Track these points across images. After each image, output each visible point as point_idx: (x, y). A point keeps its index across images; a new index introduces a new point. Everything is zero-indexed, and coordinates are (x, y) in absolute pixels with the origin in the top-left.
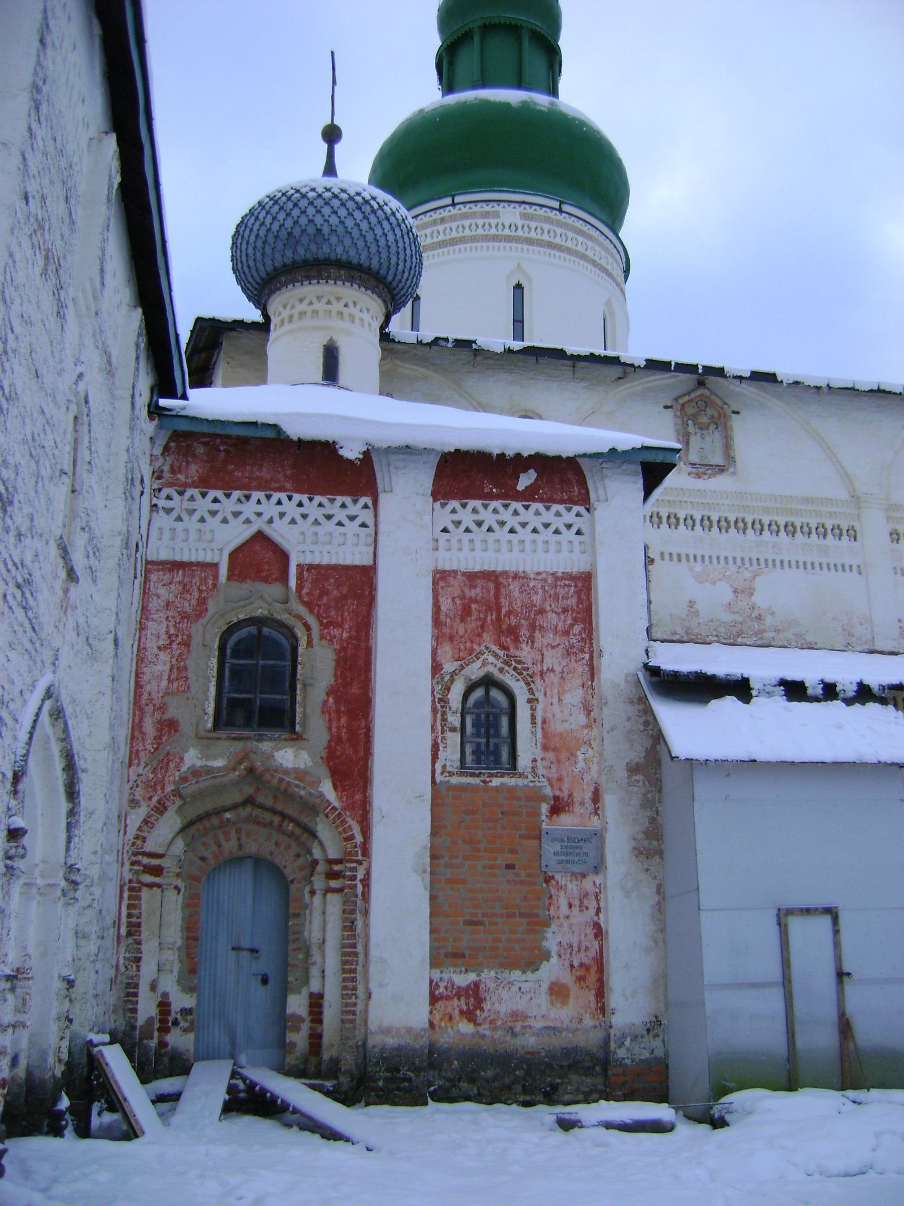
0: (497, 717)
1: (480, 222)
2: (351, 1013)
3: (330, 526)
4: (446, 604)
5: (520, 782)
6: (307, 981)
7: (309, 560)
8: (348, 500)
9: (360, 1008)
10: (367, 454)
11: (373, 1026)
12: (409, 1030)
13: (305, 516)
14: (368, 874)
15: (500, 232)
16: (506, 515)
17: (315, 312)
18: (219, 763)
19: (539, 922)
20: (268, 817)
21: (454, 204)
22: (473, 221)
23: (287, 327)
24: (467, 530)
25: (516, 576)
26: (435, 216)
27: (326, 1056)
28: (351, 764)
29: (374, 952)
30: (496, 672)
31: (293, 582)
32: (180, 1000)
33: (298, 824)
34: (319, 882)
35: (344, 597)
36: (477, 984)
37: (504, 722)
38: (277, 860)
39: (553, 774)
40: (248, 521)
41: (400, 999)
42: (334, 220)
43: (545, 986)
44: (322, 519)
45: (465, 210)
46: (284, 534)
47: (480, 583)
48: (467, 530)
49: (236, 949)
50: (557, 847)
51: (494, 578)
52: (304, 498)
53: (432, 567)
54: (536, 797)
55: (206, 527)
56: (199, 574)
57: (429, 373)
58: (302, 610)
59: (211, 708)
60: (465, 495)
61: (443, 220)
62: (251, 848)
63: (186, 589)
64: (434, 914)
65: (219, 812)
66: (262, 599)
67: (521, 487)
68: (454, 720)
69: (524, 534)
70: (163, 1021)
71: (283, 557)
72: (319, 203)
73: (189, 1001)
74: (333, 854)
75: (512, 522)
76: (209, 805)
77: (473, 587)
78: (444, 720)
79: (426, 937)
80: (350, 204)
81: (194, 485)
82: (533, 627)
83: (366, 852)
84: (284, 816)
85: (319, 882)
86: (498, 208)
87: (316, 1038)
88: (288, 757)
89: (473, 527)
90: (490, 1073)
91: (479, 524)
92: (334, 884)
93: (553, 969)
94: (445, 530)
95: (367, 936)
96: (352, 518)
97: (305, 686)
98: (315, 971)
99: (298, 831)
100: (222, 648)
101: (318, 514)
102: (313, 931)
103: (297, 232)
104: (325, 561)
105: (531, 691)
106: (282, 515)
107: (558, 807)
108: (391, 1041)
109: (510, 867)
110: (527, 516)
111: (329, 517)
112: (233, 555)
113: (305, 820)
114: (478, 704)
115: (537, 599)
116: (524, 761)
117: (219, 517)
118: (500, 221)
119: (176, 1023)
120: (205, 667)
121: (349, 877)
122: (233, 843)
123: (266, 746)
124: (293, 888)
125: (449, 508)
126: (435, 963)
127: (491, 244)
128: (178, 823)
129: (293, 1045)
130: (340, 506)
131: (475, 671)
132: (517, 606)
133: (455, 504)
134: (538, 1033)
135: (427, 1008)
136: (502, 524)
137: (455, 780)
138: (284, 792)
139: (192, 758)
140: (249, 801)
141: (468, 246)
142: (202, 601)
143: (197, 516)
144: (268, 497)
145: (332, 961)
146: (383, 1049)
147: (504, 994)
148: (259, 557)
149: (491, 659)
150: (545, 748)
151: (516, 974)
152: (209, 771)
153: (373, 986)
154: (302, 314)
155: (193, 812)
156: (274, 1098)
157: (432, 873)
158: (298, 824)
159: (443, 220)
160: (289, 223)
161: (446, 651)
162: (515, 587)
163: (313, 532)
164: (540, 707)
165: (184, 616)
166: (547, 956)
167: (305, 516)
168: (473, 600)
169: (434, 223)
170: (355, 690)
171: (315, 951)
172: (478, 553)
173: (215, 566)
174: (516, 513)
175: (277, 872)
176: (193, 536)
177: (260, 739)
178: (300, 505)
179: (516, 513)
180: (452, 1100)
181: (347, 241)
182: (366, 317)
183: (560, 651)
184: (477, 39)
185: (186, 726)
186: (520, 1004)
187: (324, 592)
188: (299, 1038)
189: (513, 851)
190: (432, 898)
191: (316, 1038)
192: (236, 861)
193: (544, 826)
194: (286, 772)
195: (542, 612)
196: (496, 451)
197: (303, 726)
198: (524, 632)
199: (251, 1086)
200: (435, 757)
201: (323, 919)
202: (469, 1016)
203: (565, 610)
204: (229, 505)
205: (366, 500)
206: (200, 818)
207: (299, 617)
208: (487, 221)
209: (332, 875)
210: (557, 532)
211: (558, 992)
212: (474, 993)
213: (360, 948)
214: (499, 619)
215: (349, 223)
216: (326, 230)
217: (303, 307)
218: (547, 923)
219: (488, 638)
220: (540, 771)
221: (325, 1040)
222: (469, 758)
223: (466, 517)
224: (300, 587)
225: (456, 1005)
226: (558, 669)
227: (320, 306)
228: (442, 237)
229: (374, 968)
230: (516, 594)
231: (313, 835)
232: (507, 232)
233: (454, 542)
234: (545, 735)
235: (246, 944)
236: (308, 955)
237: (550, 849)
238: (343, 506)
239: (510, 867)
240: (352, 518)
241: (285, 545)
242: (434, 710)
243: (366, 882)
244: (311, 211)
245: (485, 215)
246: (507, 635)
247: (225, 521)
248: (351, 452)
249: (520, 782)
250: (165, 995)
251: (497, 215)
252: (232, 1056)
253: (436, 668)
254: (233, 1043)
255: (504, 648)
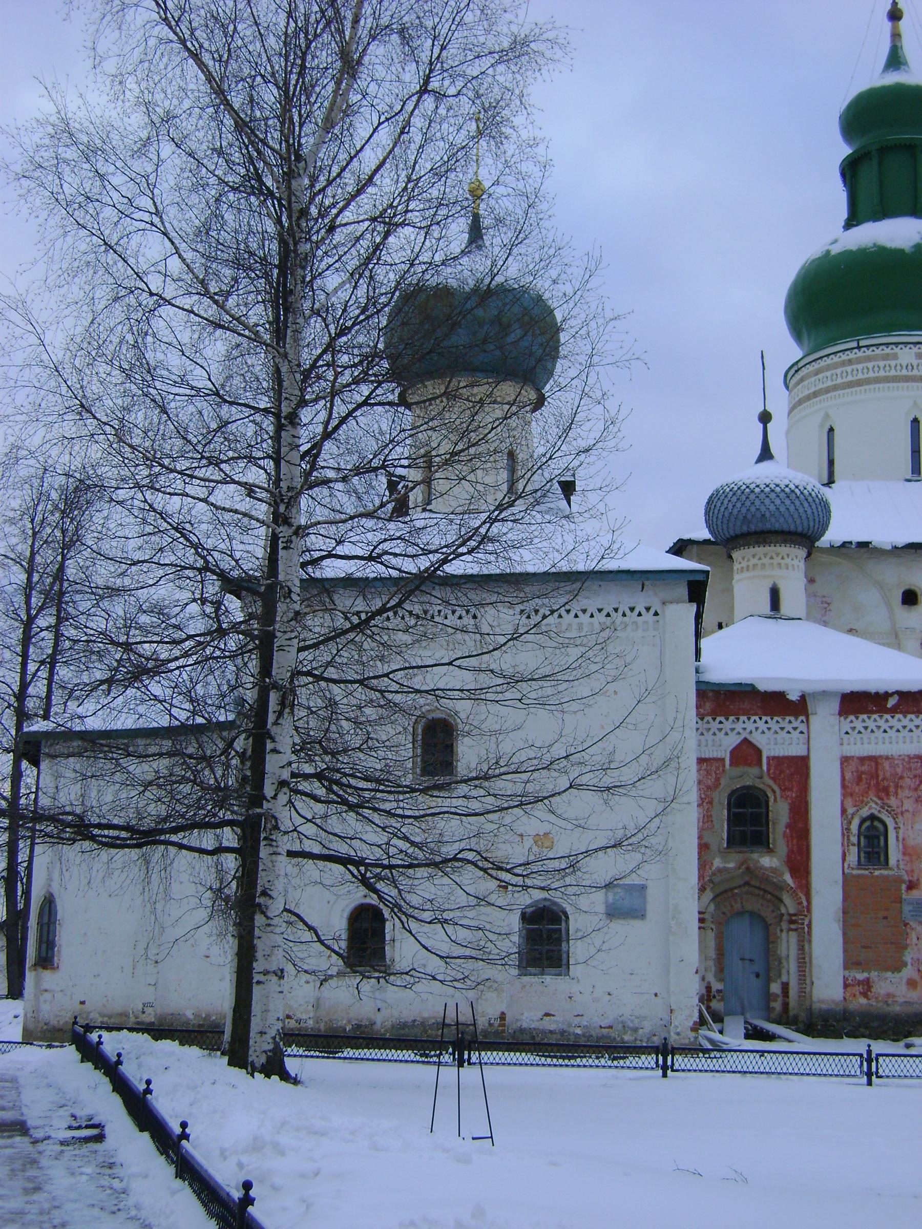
0: (878, 837)
1: (882, 364)
2: (804, 993)
3: (783, 734)
4: (848, 776)
5: (891, 873)
6: (780, 976)
7: (772, 754)
8: (792, 719)
9: (808, 990)
10: (803, 697)
11: (815, 998)
12: (833, 1001)
13: (769, 729)
14: (810, 922)
15: (899, 373)
16: (881, 722)
17: (764, 565)
18: (731, 865)
19: (901, 947)
20: (757, 891)
21: (859, 348)
22: (876, 363)
23: (746, 574)
24: (860, 732)
25: (887, 758)
26: (844, 357)
27: (791, 1013)
28: (800, 864)
29: (814, 962)
30: (876, 813)
31: (765, 767)
32: (716, 986)
33: (773, 895)
34: (784, 925)
35: (792, 774)
36: (868, 979)
37: (882, 839)
38: (763, 914)
39: (908, 868)
40: (739, 733)
41: (828, 984)
42: (772, 508)
43: (904, 980)
44: (779, 730)
45: (869, 352)
46: (759, 740)
47: (867, 762)
48: (860, 732)
49: (742, 959)
50: (911, 908)
51: (874, 760)
52: (768, 718)
53: (838, 755)
54: (899, 880)
55: (717, 738)
56: (715, 764)
57: (839, 560)
58: (770, 782)
59: (725, 836)
60: (857, 712)
61: (850, 362)
62: (749, 907)
63: (708, 773)
64: (845, 943)
65: (732, 889)
66: (749, 777)
67: (889, 706)
68: (854, 839)
69: (892, 733)
70: (708, 996)
71: (759, 752)
72: (762, 496)
73: (720, 986)
74: (792, 911)
75: (885, 726)
76: (727, 886)
77: (862, 765)
78: (848, 839)
79: (841, 954)
80: (782, 495)
81: (708, 715)
82: (897, 787)
83: (809, 910)
84: (765, 891)
85: (784, 925)
86: (896, 350)
87: (786, 1005)
88: (767, 861)
89: (862, 730)
90: (876, 1024)
91: (866, 728)
92: (793, 926)
93: (908, 972)
94: (847, 733)
95: (810, 953)
96: (795, 729)
97: (774, 823)
98: (784, 971)
99: (773, 899)
100: (729, 804)
101: (775, 727)
102: (782, 951)
103: (749, 516)
104: (781, 754)
105: (896, 823)
106: (757, 729)
107: (911, 886)
108: (824, 1007)
109: (885, 918)
110: (893, 722)
111: (782, 729)
112: (732, 752)
113: (777, 893)
114: (868, 828)
115: (899, 770)
116: (892, 861)
117: (723, 732)
118: (898, 362)
119: (714, 997)
120: (721, 814)
121: (800, 922)
122: (739, 905)
123: (755, 856)
124: (771, 928)
125: (848, 720)
126: (846, 967)
127: (891, 385)
128: (711, 896)
129: (774, 1008)
130: (788, 722)
131: (865, 812)
132: (888, 774)
133: (852, 717)
134: (901, 1005)
135: (841, 990)
136: (879, 727)
137: (855, 872)
138: (765, 879)
139: (717, 863)
140: (747, 884)
141: (872, 386)
142: (718, 780)
143: (711, 732)
144: (749, 719)
145: (793, 966)
146: (820, 1010)
147: (883, 984)
148: (746, 753)
149: (874, 806)
150: (904, 854)
151: (889, 974)
152: (725, 870)
153: (814, 979)
154: (755, 566)
155: (718, 890)
156: (768, 1031)
157: (844, 921)
158: (773, 895)
159: (850, 362)
160: (744, 510)
161: (849, 802)
162: (886, 765)
163: (775, 739)
164: (901, 831)
165: (709, 788)
166: (905, 965)
167: (769, 729)
168: (862, 773)
169: (843, 364)
170: (800, 825)
171: (784, 961)
172: (866, 745)
173: (723, 760)
174: (887, 721)
175: (763, 920)
176: (710, 743)
177: (752, 852)
178: (766, 722)
179: (887, 721)
180: (856, 1037)
181: (781, 520)
182: (796, 562)
183: (912, 800)
184: (875, 162)
185: (714, 847)
186: (891, 989)
187: (782, 772)
188: (777, 1005)
189: (887, 910)
190: (844, 934)
191: (786, 1005)
192: (740, 914)
193: (904, 896)
194: (766, 869)
195: (902, 778)
196: (873, 691)
197: (774, 844)
198: (892, 789)
199: (755, 1027)
200: (844, 860)
201: (788, 944)
202: (865, 995)
203: (915, 777)
204: (728, 725)
205: (803, 718)
206: (722, 893)
207: (769, 786)
208: (887, 363)
209: (791, 922)
210: (911, 731)
211: (912, 984)
212: (867, 983)
213: (807, 960)
214: (878, 783)
215: (782, 509)
216: (767, 515)
217: (755, 561)
218: (905, 947)
219: (872, 795)
220: (901, 867)
221: (791, 1005)
222: (862, 859)
223: (859, 725)
224: (768, 769)
225: (857, 989)
226: (911, 810)
227: (766, 561)
228: (850, 378)
229: (814, 970)
230: (887, 768)
231: (781, 901)
232: (904, 372)
233: (852, 740)
234: (904, 847)
235: (747, 957)
236: (780, 962)
237: (907, 909)
238: (790, 722)
239: (885, 918)
240: (795, 729)
241: (760, 747)
242: (843, 835)
243: (809, 925)
244: (757, 502)
245: (886, 357)
246: (883, 791)
247: (726, 734)
248: (793, 697)
249: (891, 873)
250: (709, 983)
251: (895, 357)
252: (743, 1014)
253: (844, 811)
254: (743, 1008)
255: (881, 799)
